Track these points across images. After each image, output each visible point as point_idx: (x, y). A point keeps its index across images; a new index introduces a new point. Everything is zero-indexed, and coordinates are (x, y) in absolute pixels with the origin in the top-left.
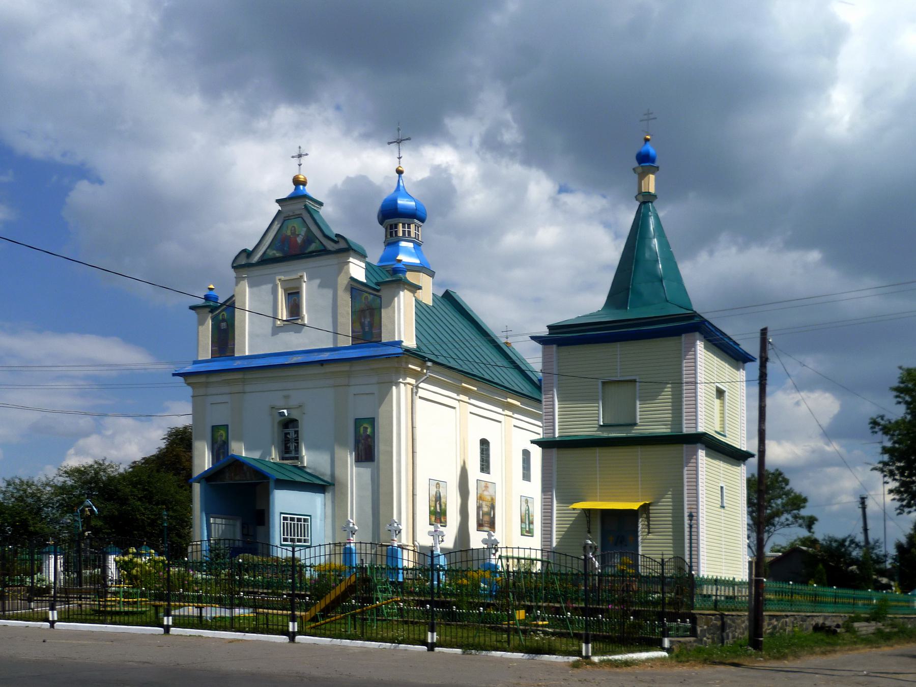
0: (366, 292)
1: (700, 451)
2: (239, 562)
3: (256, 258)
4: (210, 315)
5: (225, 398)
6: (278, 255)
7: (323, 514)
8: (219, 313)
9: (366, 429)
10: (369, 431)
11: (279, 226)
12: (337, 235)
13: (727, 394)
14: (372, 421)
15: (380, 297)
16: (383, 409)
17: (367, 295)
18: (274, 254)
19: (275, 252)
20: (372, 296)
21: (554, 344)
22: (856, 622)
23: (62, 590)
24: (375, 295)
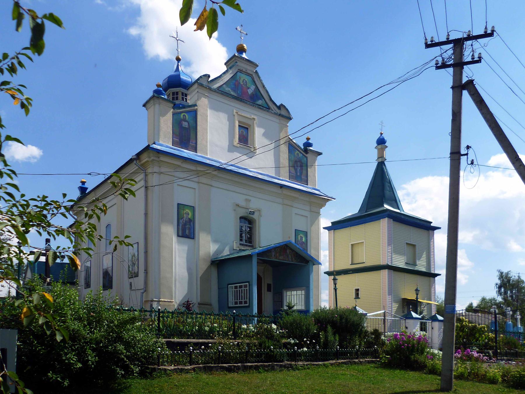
0: (298, 151)
1: (250, 93)
2: (92, 366)
3: (216, 86)
4: (172, 110)
5: (194, 185)
6: (232, 93)
7: (412, 266)
8: (181, 113)
9: (302, 238)
10: (304, 240)
11: (232, 75)
12: (282, 105)
13: (417, 246)
14: (306, 234)
15: (307, 157)
16: (313, 228)
17: (298, 152)
18: (229, 90)
19: (229, 89)
20: (301, 155)
21: (392, 219)
22: (454, 308)
23: (128, 323)
24: (303, 155)
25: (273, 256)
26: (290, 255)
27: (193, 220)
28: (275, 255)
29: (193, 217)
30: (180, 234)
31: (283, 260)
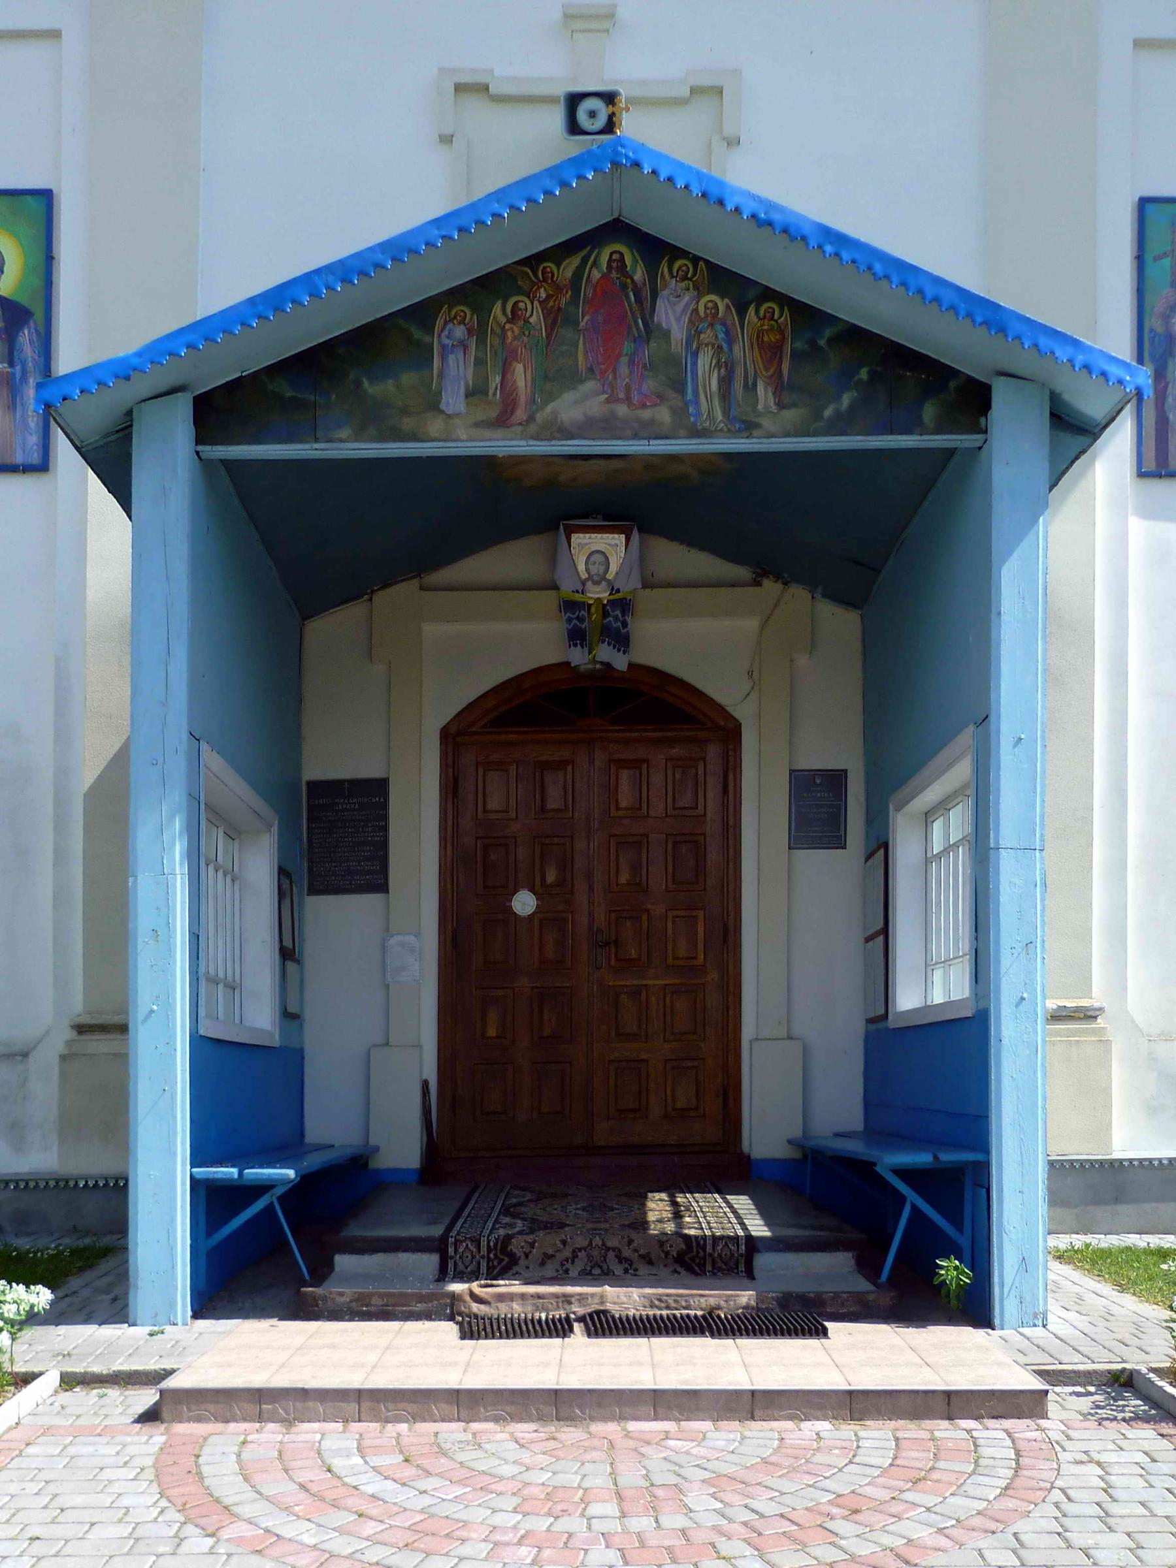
25: (453, 400)
26: (704, 361)
27: (39, 315)
28: (475, 393)
29: (37, 282)
30: (1150, 465)
31: (607, 427)
